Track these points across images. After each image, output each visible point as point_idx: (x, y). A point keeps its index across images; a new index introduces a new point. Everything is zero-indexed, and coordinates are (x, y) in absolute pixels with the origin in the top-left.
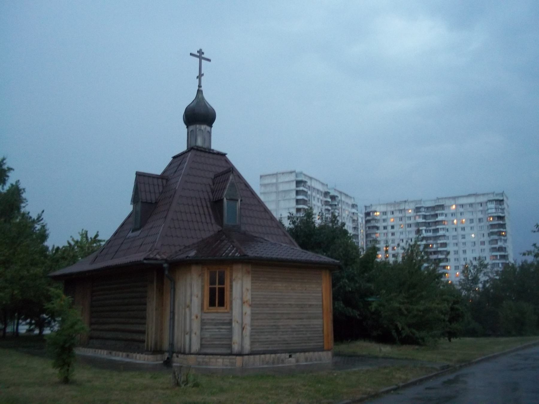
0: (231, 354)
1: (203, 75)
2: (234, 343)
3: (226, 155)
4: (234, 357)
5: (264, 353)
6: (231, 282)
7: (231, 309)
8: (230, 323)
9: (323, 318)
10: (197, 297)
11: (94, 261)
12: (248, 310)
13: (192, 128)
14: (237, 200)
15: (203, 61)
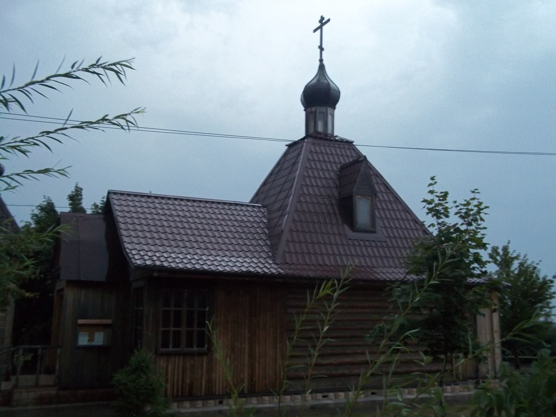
13: (309, 110)
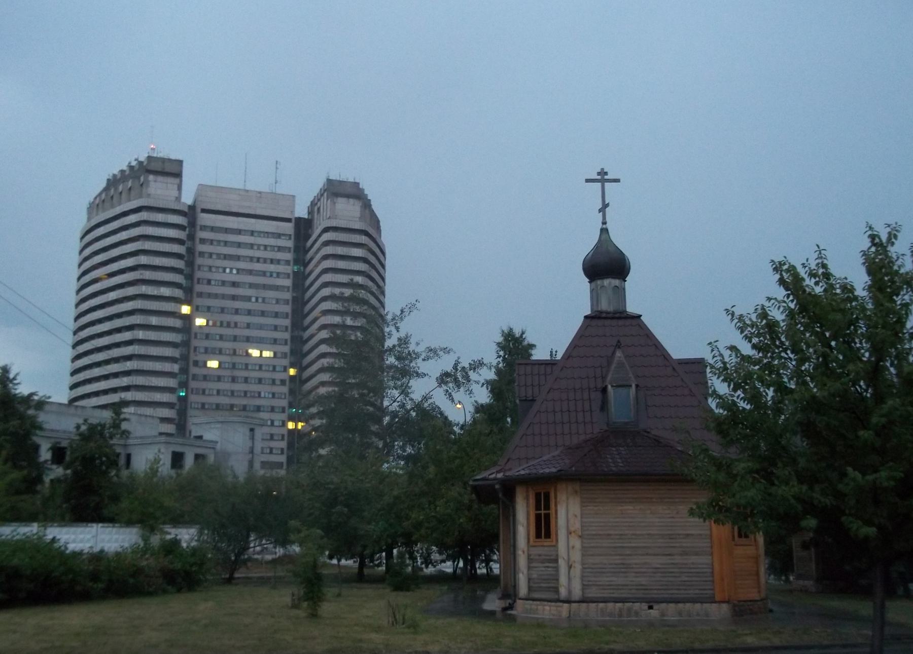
0: (558, 601)
1: (600, 211)
2: (561, 586)
3: (642, 318)
4: (561, 604)
5: (605, 601)
6: (556, 506)
7: (557, 541)
8: (556, 561)
9: (712, 554)
10: (523, 526)
12: (576, 543)
14: (631, 386)
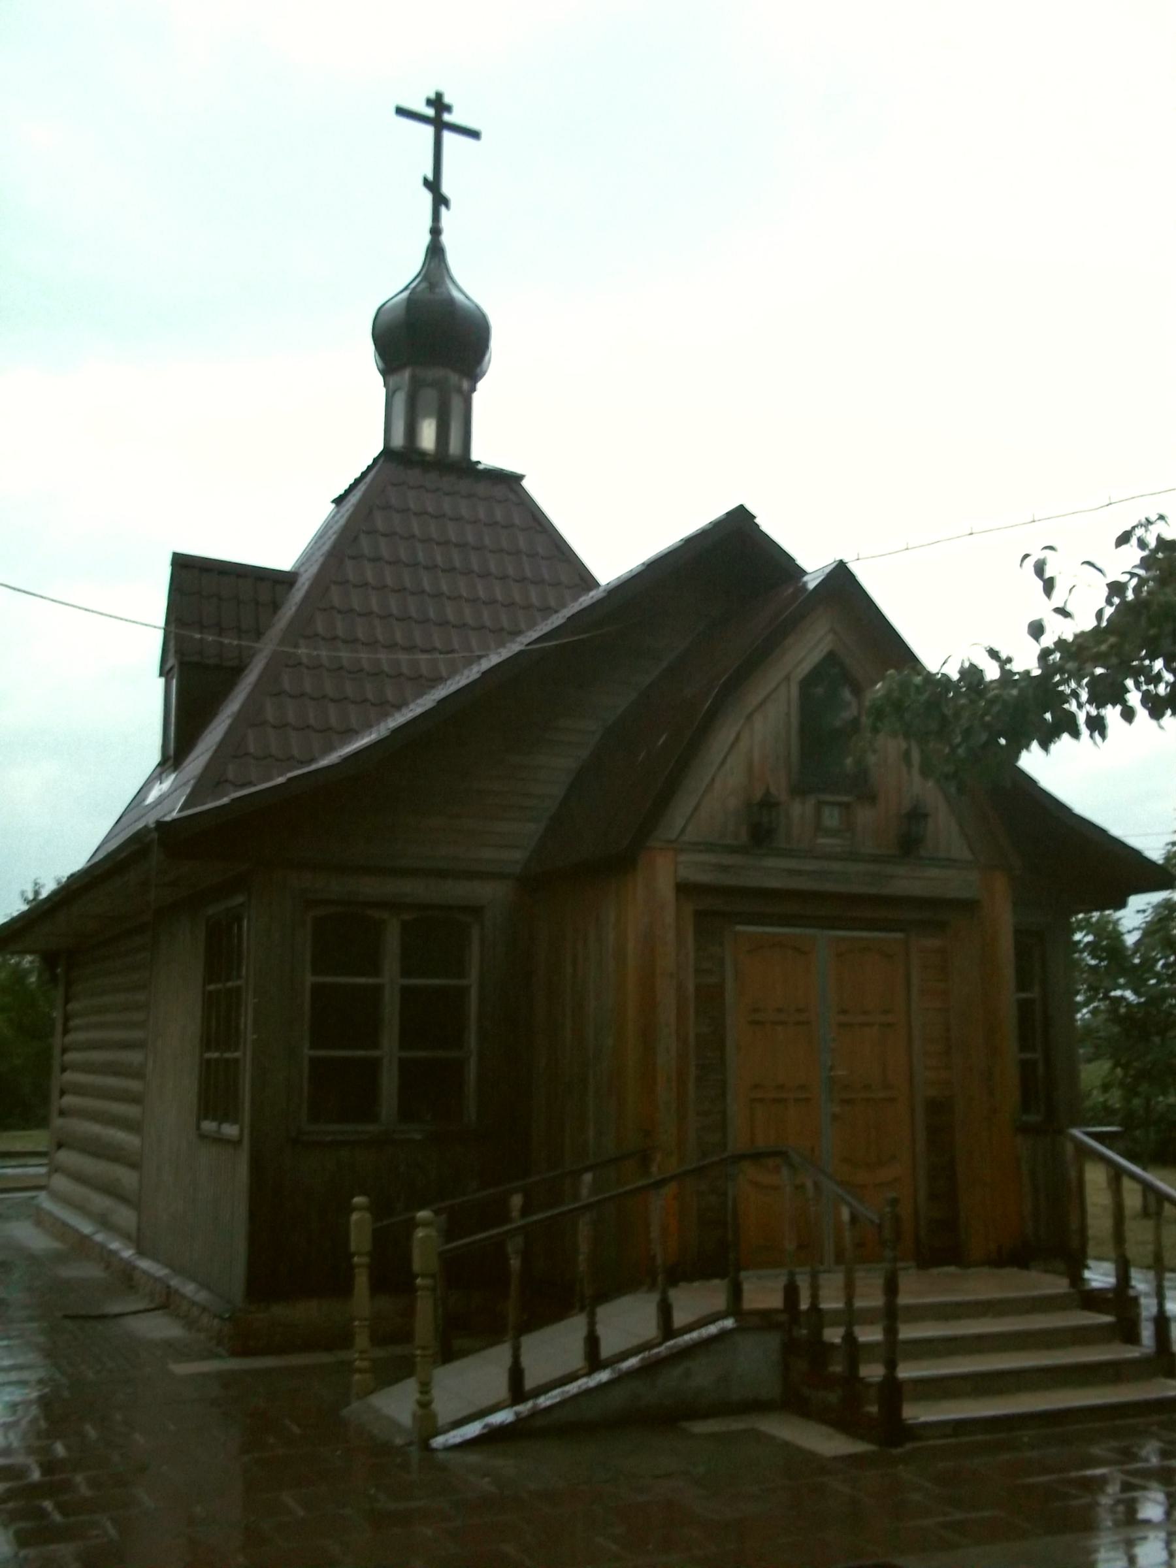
11: (449, 688)
15: (447, 136)
